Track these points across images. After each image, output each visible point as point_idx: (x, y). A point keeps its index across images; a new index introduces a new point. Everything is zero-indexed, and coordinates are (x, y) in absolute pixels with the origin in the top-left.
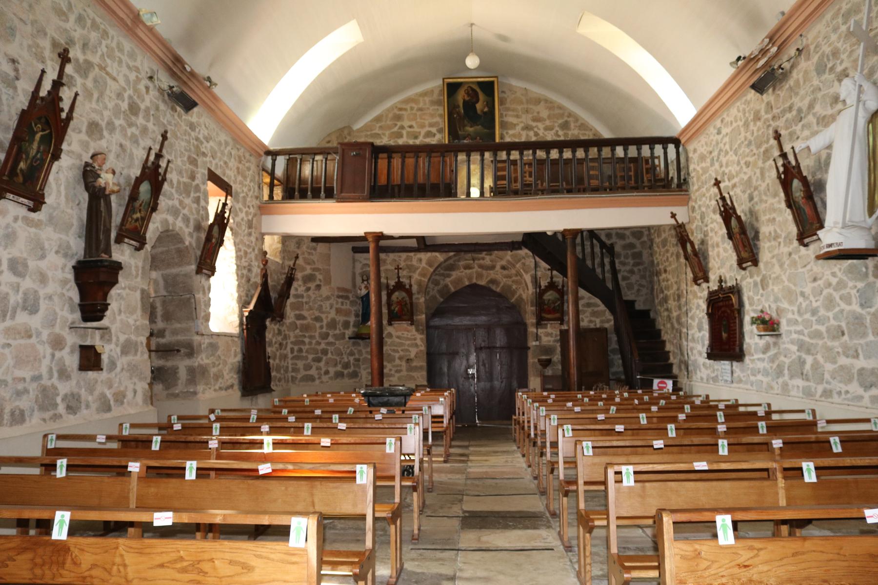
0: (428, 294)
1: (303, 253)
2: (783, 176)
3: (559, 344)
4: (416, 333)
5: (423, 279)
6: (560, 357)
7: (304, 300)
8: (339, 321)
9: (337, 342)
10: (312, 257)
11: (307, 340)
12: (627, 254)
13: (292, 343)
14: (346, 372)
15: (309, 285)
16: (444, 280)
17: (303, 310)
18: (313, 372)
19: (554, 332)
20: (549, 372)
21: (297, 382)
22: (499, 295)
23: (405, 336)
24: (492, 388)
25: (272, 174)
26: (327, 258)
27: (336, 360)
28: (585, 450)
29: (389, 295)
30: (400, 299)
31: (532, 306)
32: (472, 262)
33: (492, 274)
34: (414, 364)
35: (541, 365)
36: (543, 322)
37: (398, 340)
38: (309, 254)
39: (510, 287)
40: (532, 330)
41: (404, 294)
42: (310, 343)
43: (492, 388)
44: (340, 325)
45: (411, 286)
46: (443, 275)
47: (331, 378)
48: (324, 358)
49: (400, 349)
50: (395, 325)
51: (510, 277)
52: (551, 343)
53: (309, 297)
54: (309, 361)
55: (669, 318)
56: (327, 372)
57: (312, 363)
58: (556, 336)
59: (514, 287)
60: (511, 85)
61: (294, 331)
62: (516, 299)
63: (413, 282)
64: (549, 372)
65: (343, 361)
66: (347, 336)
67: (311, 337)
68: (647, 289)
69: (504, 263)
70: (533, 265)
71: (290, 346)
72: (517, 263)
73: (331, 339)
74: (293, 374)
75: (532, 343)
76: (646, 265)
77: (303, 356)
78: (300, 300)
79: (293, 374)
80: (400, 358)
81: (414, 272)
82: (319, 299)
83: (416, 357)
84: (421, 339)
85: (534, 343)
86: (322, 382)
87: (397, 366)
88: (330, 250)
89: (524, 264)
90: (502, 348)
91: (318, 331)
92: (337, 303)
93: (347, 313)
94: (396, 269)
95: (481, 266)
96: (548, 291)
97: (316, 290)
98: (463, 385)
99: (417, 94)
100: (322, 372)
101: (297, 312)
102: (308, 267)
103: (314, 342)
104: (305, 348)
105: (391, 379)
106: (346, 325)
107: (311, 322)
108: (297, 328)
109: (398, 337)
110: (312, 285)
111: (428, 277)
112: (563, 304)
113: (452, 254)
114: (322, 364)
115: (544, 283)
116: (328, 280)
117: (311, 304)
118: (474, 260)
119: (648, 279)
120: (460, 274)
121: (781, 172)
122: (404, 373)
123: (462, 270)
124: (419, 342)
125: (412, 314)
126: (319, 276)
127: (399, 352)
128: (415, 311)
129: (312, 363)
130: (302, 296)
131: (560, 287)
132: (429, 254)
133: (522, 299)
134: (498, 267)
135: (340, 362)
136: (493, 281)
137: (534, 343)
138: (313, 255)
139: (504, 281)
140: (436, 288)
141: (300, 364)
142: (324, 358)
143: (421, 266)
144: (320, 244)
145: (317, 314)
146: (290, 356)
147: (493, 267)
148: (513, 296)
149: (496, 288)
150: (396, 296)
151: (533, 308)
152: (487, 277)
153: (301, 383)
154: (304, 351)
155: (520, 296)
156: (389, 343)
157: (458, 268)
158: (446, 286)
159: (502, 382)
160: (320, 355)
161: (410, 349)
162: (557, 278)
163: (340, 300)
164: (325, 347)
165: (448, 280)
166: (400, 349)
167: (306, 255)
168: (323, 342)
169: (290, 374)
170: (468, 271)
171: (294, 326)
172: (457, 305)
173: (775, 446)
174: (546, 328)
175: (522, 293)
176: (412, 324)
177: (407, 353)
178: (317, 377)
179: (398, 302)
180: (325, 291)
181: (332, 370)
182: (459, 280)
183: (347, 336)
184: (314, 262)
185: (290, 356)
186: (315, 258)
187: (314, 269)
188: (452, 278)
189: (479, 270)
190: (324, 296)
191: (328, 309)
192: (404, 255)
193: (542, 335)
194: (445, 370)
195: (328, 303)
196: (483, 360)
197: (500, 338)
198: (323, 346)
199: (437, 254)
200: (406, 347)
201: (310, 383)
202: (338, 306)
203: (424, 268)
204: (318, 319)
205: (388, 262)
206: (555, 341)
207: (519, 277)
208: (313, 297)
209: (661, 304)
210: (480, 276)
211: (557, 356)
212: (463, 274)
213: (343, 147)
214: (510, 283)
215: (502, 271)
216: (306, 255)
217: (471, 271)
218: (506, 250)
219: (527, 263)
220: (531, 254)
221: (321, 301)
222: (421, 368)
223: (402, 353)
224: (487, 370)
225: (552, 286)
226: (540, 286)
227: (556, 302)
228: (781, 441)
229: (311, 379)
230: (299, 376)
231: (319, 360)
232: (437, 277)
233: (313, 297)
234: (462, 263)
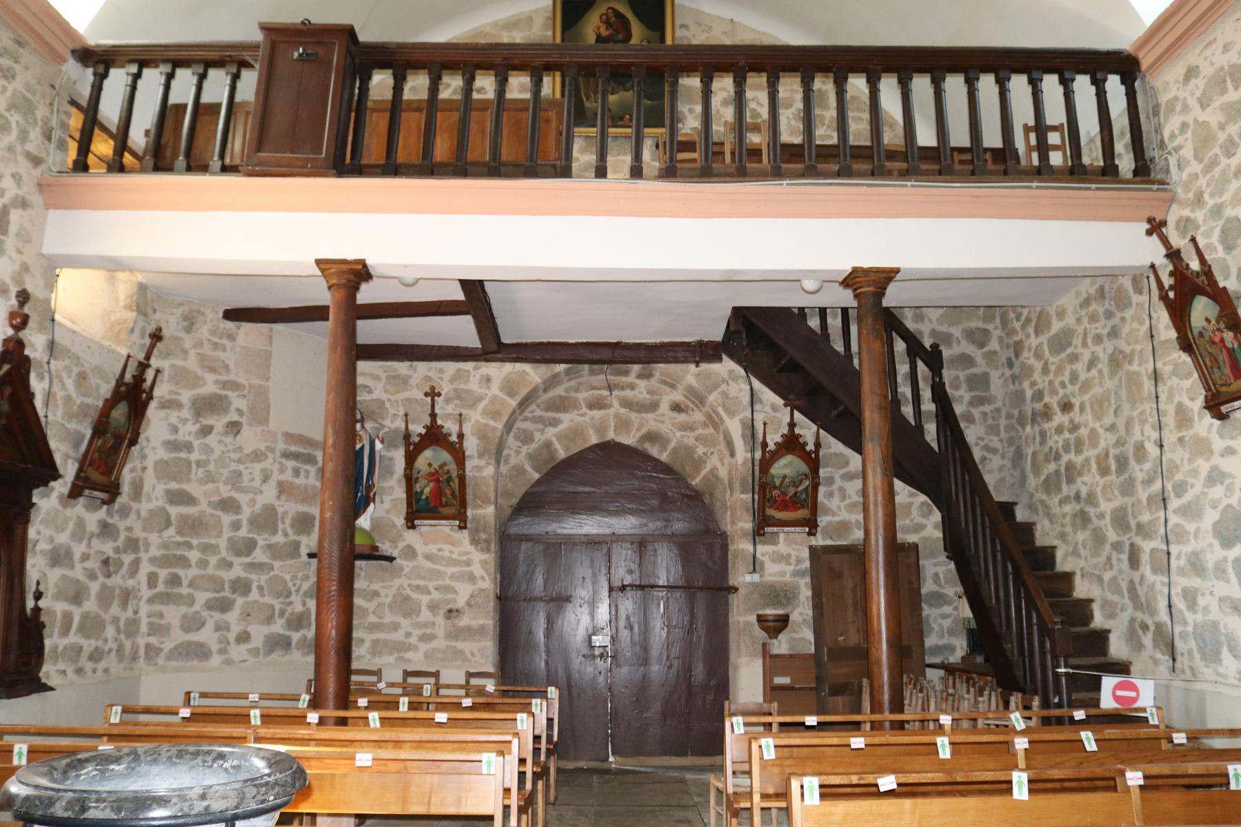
0: (506, 462)
1: (200, 344)
2: (1171, 295)
3: (808, 580)
4: (471, 549)
5: (492, 423)
6: (810, 612)
7: (194, 456)
8: (285, 513)
9: (277, 564)
10: (221, 355)
11: (194, 556)
12: (957, 377)
13: (152, 560)
14: (296, 637)
15: (208, 421)
16: (542, 431)
17: (189, 480)
18: (207, 636)
19: (794, 554)
20: (781, 646)
21: (161, 661)
22: (666, 469)
23: (446, 554)
24: (645, 680)
25: (91, 112)
26: (263, 361)
27: (272, 607)
28: (765, 751)
29: (411, 458)
30: (436, 466)
31: (742, 492)
32: (606, 393)
33: (651, 422)
34: (464, 621)
35: (763, 628)
36: (768, 529)
37: (428, 565)
38: (216, 346)
39: (690, 451)
40: (742, 546)
41: (445, 456)
42: (203, 564)
43: (645, 680)
44: (288, 521)
45: (461, 436)
46: (540, 420)
47: (255, 652)
48: (240, 601)
49: (431, 585)
50: (423, 529)
51: (692, 429)
52: (788, 578)
53: (208, 450)
54: (197, 607)
55: (1082, 519)
56: (244, 637)
57: (205, 614)
58: (799, 561)
59: (700, 450)
60: (700, 12)
61: (160, 532)
62: (705, 478)
63: (467, 429)
64: (781, 646)
65: (290, 609)
66: (304, 551)
67: (206, 548)
68: (1003, 457)
69: (678, 396)
70: (746, 399)
71: (145, 569)
72: (710, 392)
73: (259, 556)
74: (152, 640)
75: (742, 578)
76: (999, 404)
77: (180, 596)
78: (183, 455)
79: (152, 640)
80: (433, 607)
81: (472, 406)
82: (235, 456)
83: (469, 605)
84: (484, 563)
85: (748, 578)
86: (229, 662)
87: (425, 625)
88: (271, 342)
89: (725, 395)
90: (669, 587)
91: (227, 533)
92: (282, 470)
93: (305, 496)
94: (426, 395)
95: (626, 404)
96: (782, 456)
97: (226, 433)
98: (579, 672)
99: (496, 24)
100: (232, 636)
101: (174, 486)
102: (210, 378)
103: (213, 560)
104: (186, 575)
105: (409, 655)
106: (303, 523)
107: (210, 511)
108: (168, 523)
109: (429, 557)
110: (218, 423)
111: (505, 418)
112: (815, 486)
113: (561, 367)
114: (232, 617)
115: (774, 439)
116: (261, 413)
117: (211, 467)
118: (610, 388)
119: (1003, 435)
120: (578, 419)
121: (1167, 286)
122: (441, 643)
123: (585, 410)
124: (477, 570)
125: (463, 504)
126: (238, 401)
127: (429, 593)
128: (469, 498)
129: (205, 614)
130: (188, 447)
131: (810, 447)
132: (508, 367)
133: (717, 477)
134: (664, 407)
135: (282, 613)
136: (652, 437)
137: (748, 578)
138: (224, 350)
139: (677, 437)
140: (524, 449)
141: (173, 614)
142: (240, 601)
143: (490, 394)
144: (246, 326)
145: (226, 492)
146: (146, 593)
147: (653, 407)
148: (698, 472)
149: (661, 452)
150: (429, 458)
151: (747, 497)
152: (639, 429)
153: (173, 664)
154: (185, 582)
155: (713, 472)
156: (406, 570)
157: (575, 405)
158: (548, 445)
159: (670, 667)
160: (227, 593)
161: (458, 586)
162: (802, 427)
163: (291, 464)
164: (243, 574)
165: (551, 432)
166: (431, 585)
167: (207, 349)
168: (237, 561)
169: (142, 641)
170: (596, 414)
171: (161, 520)
172: (571, 488)
173: (1130, 783)
174: (775, 543)
175: (718, 464)
176: (462, 527)
177: (449, 596)
178: (215, 647)
179: (430, 475)
180: (250, 438)
181: (259, 633)
182: (577, 432)
183: (304, 551)
184: (227, 367)
185: (146, 593)
186: (229, 357)
187: (224, 385)
188: (561, 427)
189: (623, 411)
190: (247, 451)
191: (257, 483)
192: (450, 367)
193: (766, 559)
194: (540, 635)
195: (257, 467)
196: (628, 617)
197: (666, 567)
198: (237, 571)
199: (527, 367)
200: (448, 582)
201: (195, 663)
202: (283, 478)
203: (494, 399)
204: (228, 505)
205: (413, 382)
206: (797, 574)
207: (712, 430)
208: (218, 450)
209: (1051, 485)
210: (623, 425)
211: (800, 609)
212: (587, 419)
213: (274, 37)
214: (691, 441)
215: (675, 414)
216: (207, 349)
217: (603, 412)
218: (686, 361)
219: (732, 394)
220: (742, 372)
221: (240, 461)
222: (481, 630)
223: (436, 595)
224: (636, 638)
225: (791, 443)
226: (764, 445)
227: (801, 482)
228: (1140, 774)
229: (202, 652)
230: (168, 645)
231: (224, 606)
232: (528, 425)
233: (218, 450)
234: (583, 396)
